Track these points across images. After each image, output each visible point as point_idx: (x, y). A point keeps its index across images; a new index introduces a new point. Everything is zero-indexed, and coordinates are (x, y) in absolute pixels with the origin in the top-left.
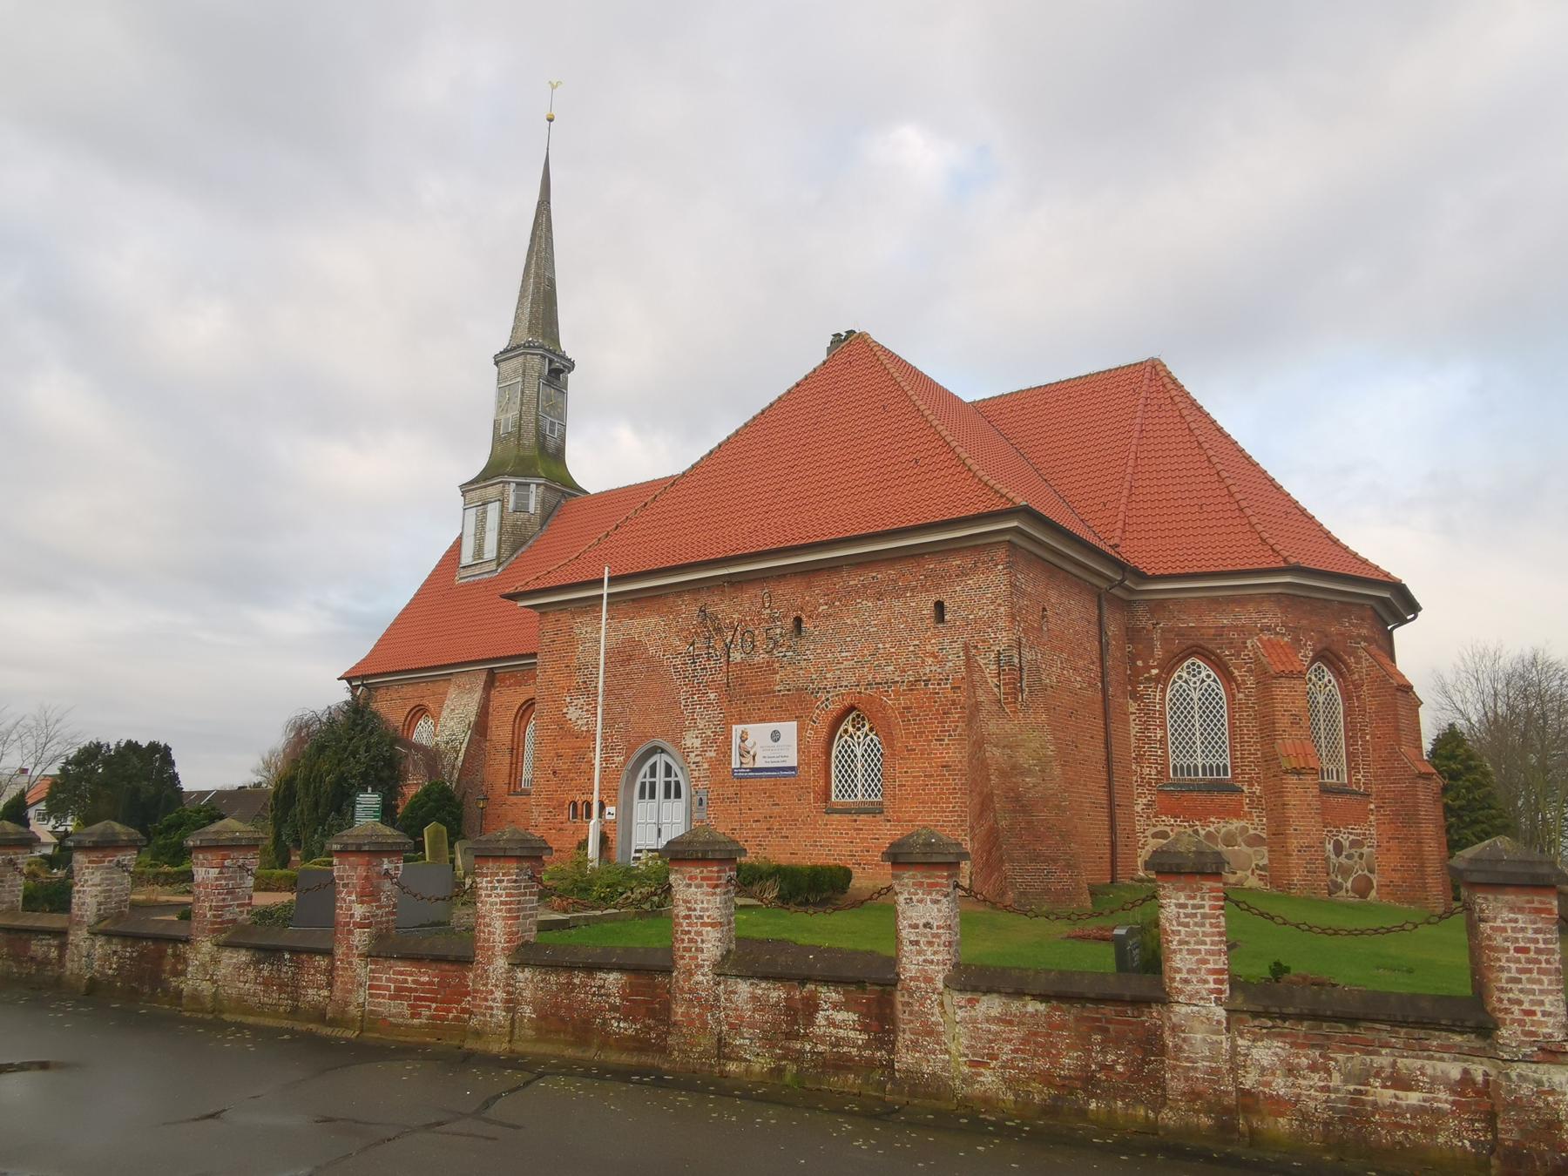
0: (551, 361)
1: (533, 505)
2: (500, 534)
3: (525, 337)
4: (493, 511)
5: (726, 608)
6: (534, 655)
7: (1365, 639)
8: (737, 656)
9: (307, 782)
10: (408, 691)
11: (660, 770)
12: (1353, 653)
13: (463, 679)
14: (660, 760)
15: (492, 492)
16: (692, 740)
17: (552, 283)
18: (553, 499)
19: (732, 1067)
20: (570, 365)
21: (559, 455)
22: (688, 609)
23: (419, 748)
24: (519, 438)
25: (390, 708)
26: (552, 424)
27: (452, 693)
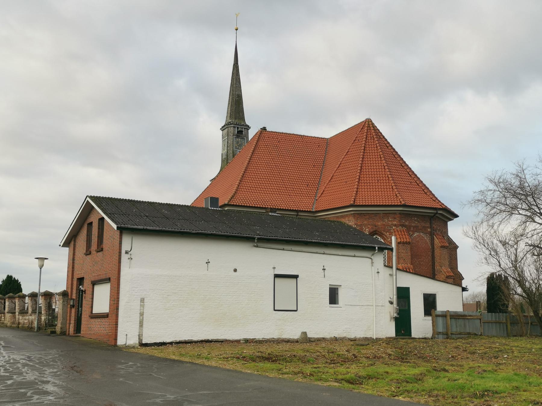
0: (238, 128)
7: (395, 225)
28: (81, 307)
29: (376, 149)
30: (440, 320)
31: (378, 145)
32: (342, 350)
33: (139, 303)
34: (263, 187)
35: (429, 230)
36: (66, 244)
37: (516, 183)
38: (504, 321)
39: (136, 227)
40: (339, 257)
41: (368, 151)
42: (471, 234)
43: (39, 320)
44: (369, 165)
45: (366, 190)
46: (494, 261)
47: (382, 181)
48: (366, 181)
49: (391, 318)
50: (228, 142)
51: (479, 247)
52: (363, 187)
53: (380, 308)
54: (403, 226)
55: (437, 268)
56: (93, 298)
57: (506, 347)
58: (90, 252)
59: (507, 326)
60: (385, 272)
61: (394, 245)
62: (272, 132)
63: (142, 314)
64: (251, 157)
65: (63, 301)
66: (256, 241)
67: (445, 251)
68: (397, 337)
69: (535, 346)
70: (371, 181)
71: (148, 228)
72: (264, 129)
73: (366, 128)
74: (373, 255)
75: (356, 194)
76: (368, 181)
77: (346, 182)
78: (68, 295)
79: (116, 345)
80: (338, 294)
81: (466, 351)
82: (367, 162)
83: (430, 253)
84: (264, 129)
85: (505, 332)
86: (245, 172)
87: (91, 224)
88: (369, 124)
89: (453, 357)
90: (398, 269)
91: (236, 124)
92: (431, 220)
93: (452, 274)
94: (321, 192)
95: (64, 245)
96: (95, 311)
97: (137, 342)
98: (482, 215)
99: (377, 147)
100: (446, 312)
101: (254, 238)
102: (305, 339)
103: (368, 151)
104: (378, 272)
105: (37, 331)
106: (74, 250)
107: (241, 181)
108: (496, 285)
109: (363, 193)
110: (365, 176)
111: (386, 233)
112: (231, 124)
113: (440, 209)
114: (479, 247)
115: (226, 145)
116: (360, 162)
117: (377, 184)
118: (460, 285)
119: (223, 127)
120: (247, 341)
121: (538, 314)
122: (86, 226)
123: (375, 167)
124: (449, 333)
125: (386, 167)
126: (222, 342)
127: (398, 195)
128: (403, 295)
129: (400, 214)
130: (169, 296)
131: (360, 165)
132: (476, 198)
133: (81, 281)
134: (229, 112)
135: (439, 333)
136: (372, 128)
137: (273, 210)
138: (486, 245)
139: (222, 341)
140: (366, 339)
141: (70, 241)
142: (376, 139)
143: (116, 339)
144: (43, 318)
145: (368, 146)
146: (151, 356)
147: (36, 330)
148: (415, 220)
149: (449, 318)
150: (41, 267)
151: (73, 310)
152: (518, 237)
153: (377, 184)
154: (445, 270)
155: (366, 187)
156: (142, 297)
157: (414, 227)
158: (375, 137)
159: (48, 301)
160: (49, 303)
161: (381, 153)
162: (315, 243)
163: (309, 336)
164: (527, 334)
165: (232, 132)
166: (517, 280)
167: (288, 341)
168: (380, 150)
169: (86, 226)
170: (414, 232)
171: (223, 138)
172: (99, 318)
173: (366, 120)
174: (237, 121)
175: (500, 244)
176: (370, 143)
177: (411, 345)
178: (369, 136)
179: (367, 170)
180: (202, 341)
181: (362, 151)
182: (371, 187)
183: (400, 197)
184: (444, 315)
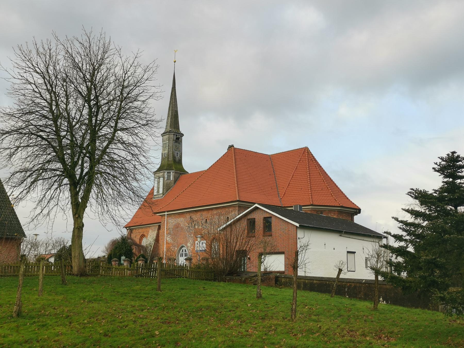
0: (176, 135)
1: (172, 178)
2: (163, 186)
3: (169, 129)
4: (161, 180)
5: (196, 217)
6: (160, 223)
8: (196, 227)
9: (114, 255)
10: (140, 230)
11: (184, 251)
13: (153, 228)
14: (184, 248)
15: (161, 174)
16: (189, 245)
17: (176, 112)
18: (177, 175)
19: (106, 257)
21: (179, 162)
22: (188, 216)
23: (143, 247)
24: (168, 158)
25: (136, 237)
26: (177, 153)
27: (150, 231)
72: (233, 146)
84: (183, 135)
101: (342, 231)
165: (172, 138)
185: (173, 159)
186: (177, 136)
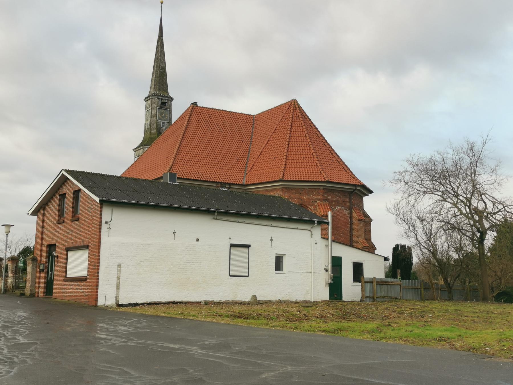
0: (162, 99)
7: (319, 200)
12: (313, 205)
20: (171, 99)
26: (163, 123)
28: (51, 271)
29: (301, 128)
30: (368, 286)
31: (303, 124)
32: (294, 310)
33: (116, 268)
34: (197, 160)
35: (348, 204)
36: (35, 212)
37: (430, 166)
38: (419, 287)
39: (115, 200)
40: (291, 230)
41: (294, 130)
42: (394, 212)
43: (6, 283)
44: (296, 143)
45: (293, 166)
46: (412, 235)
47: (307, 159)
48: (292, 158)
49: (326, 284)
50: (151, 113)
51: (400, 222)
52: (290, 163)
53: (317, 274)
54: (325, 200)
55: (355, 239)
56: (67, 264)
57: (426, 308)
58: (64, 221)
59: (421, 291)
60: (322, 243)
61: (330, 219)
62: (203, 107)
63: (119, 278)
64: (185, 131)
65: (33, 266)
66: (216, 214)
67: (362, 224)
68: (331, 300)
69: (450, 308)
70: (297, 158)
71: (126, 201)
72: (195, 104)
73: (292, 108)
74: (312, 228)
75: (284, 170)
76: (295, 158)
77: (274, 158)
78: (37, 260)
79: (96, 305)
80: (282, 262)
81: (395, 311)
82: (293, 140)
83: (349, 226)
84: (195, 104)
85: (420, 296)
86: (180, 146)
87: (64, 195)
88: (295, 105)
89: (385, 316)
90: (333, 241)
91: (160, 96)
92: (350, 195)
93: (367, 245)
94: (251, 167)
95: (32, 214)
96: (69, 275)
97: (115, 303)
98: (400, 194)
99: (302, 127)
100: (373, 278)
101: (214, 212)
102: (255, 302)
103: (294, 130)
104: (316, 243)
105: (3, 293)
106: (43, 218)
107: (177, 154)
108: (401, 256)
109: (291, 169)
110: (292, 153)
111: (311, 206)
112: (156, 95)
113: (359, 186)
114: (400, 222)
115: (150, 116)
116: (288, 140)
117: (303, 161)
118: (373, 253)
119: (146, 98)
120: (207, 303)
121: (447, 280)
122: (57, 197)
123: (301, 145)
124: (375, 297)
125: (311, 146)
126: (186, 303)
127: (322, 172)
128: (337, 262)
129: (323, 189)
130: (150, 261)
131: (287, 143)
132: (397, 178)
133: (51, 247)
134: (153, 83)
135: (367, 297)
136: (298, 109)
137: (223, 185)
138: (406, 221)
139: (186, 303)
140: (305, 302)
141: (40, 210)
142: (301, 119)
143: (96, 300)
144: (10, 281)
145: (294, 125)
146: (143, 314)
147: (2, 292)
148: (337, 195)
149: (375, 284)
150: (7, 234)
151: (43, 275)
152: (435, 214)
153: (303, 161)
154: (362, 241)
155: (293, 164)
156: (119, 262)
157: (335, 201)
158: (300, 116)
159: (15, 265)
160: (16, 267)
161: (306, 132)
162: (265, 216)
163: (259, 298)
164: (437, 299)
165: (156, 103)
166: (430, 251)
167: (241, 303)
168: (305, 130)
169: (57, 197)
170: (335, 206)
171: (146, 108)
172: (76, 281)
173: (292, 100)
174: (160, 92)
175: (418, 221)
176: (296, 123)
177: (348, 307)
178: (295, 115)
179: (294, 148)
180: (169, 303)
181: (289, 129)
182: (298, 164)
183: (324, 174)
184: (371, 281)
185: (157, 130)
186: (163, 101)
